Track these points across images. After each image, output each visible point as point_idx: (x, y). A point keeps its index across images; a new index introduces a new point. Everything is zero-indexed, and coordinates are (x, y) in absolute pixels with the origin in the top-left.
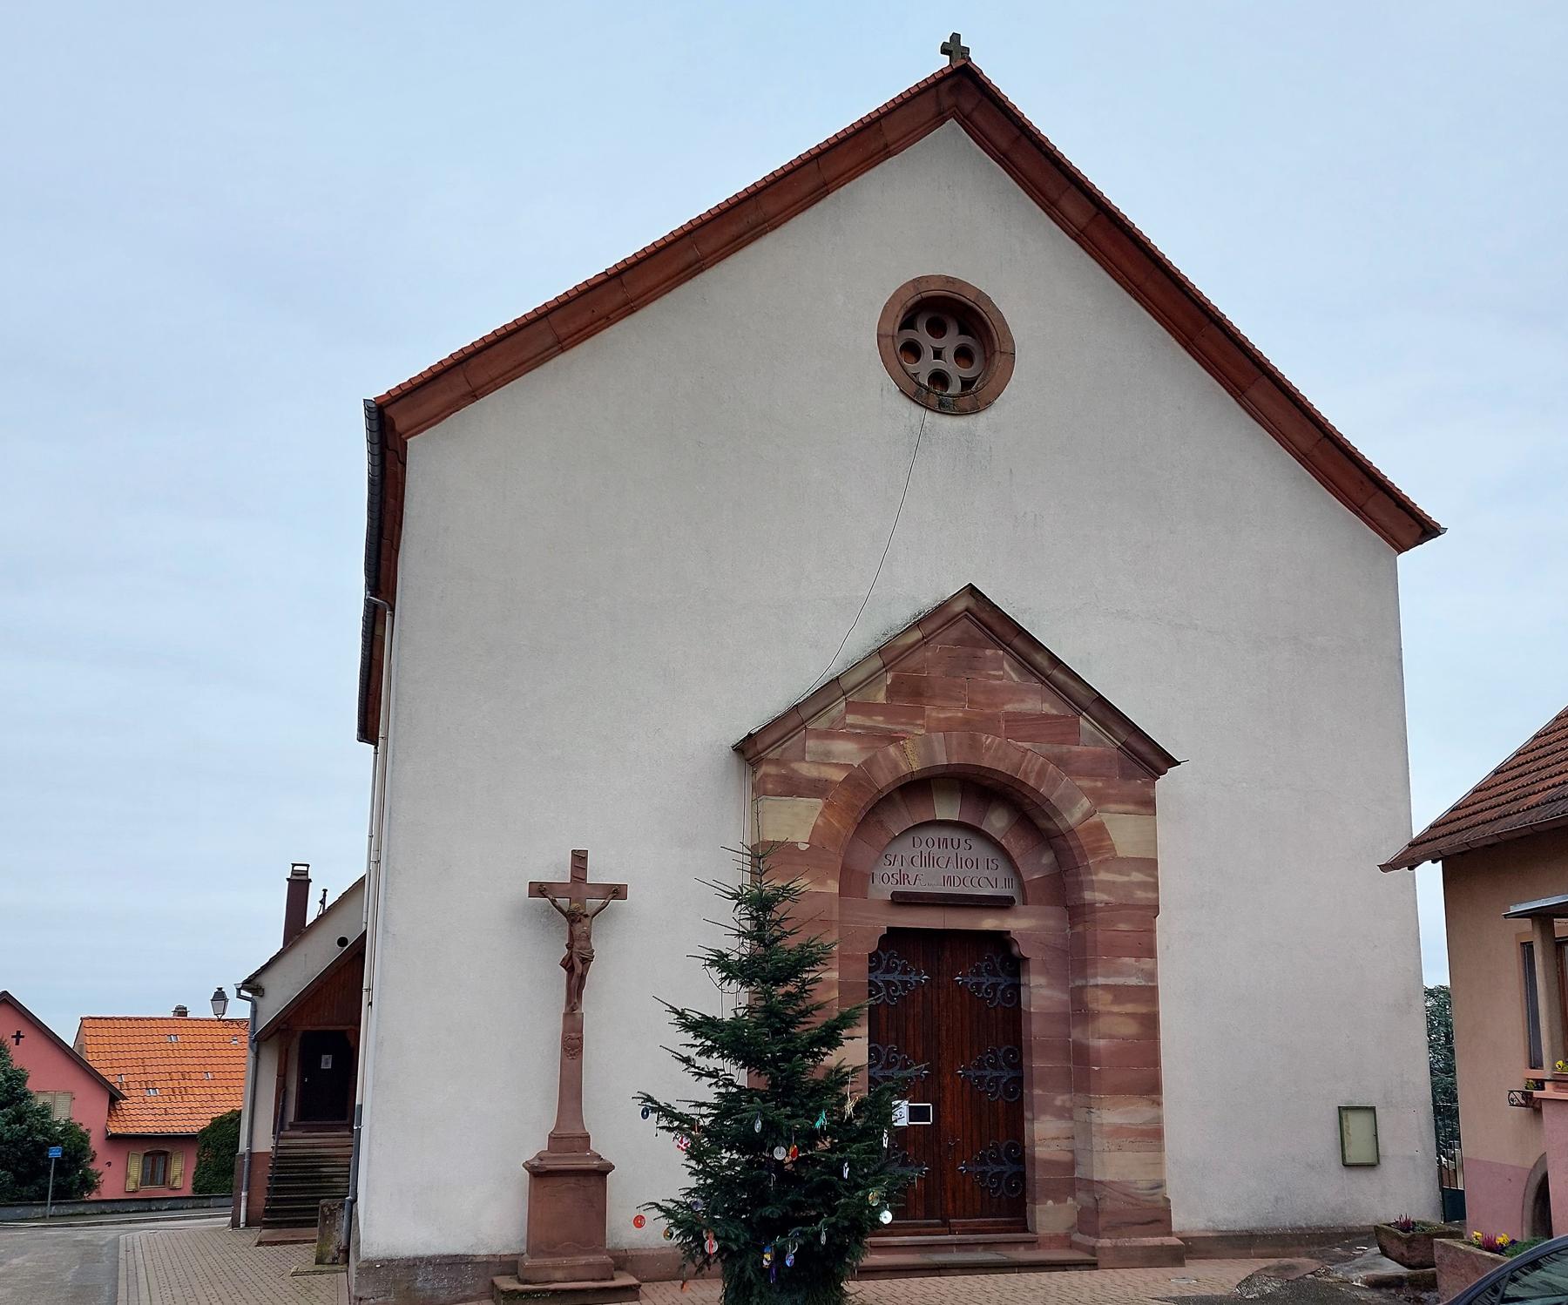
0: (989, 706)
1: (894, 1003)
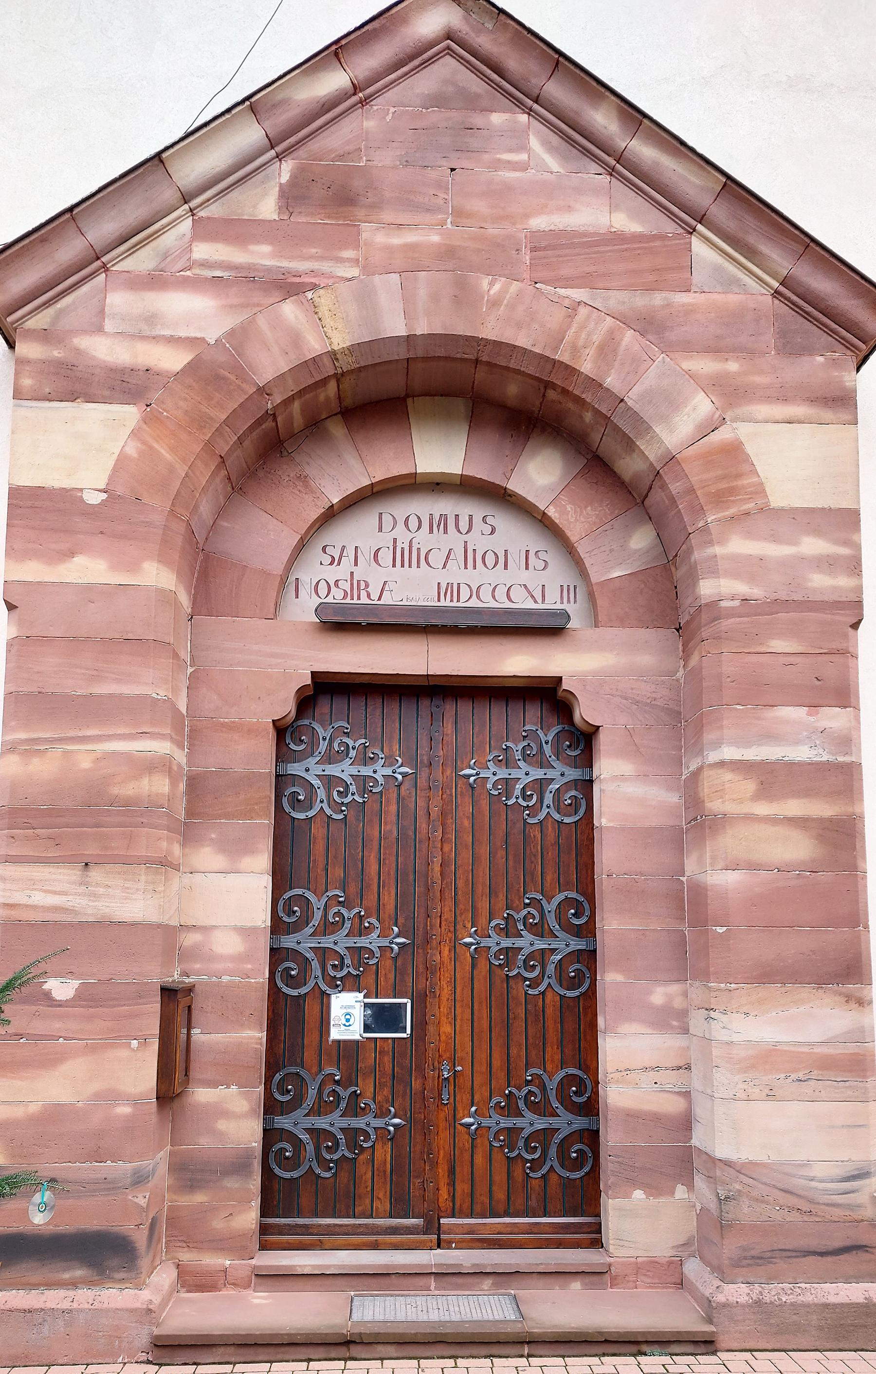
0: (497, 219)
1: (341, 816)
